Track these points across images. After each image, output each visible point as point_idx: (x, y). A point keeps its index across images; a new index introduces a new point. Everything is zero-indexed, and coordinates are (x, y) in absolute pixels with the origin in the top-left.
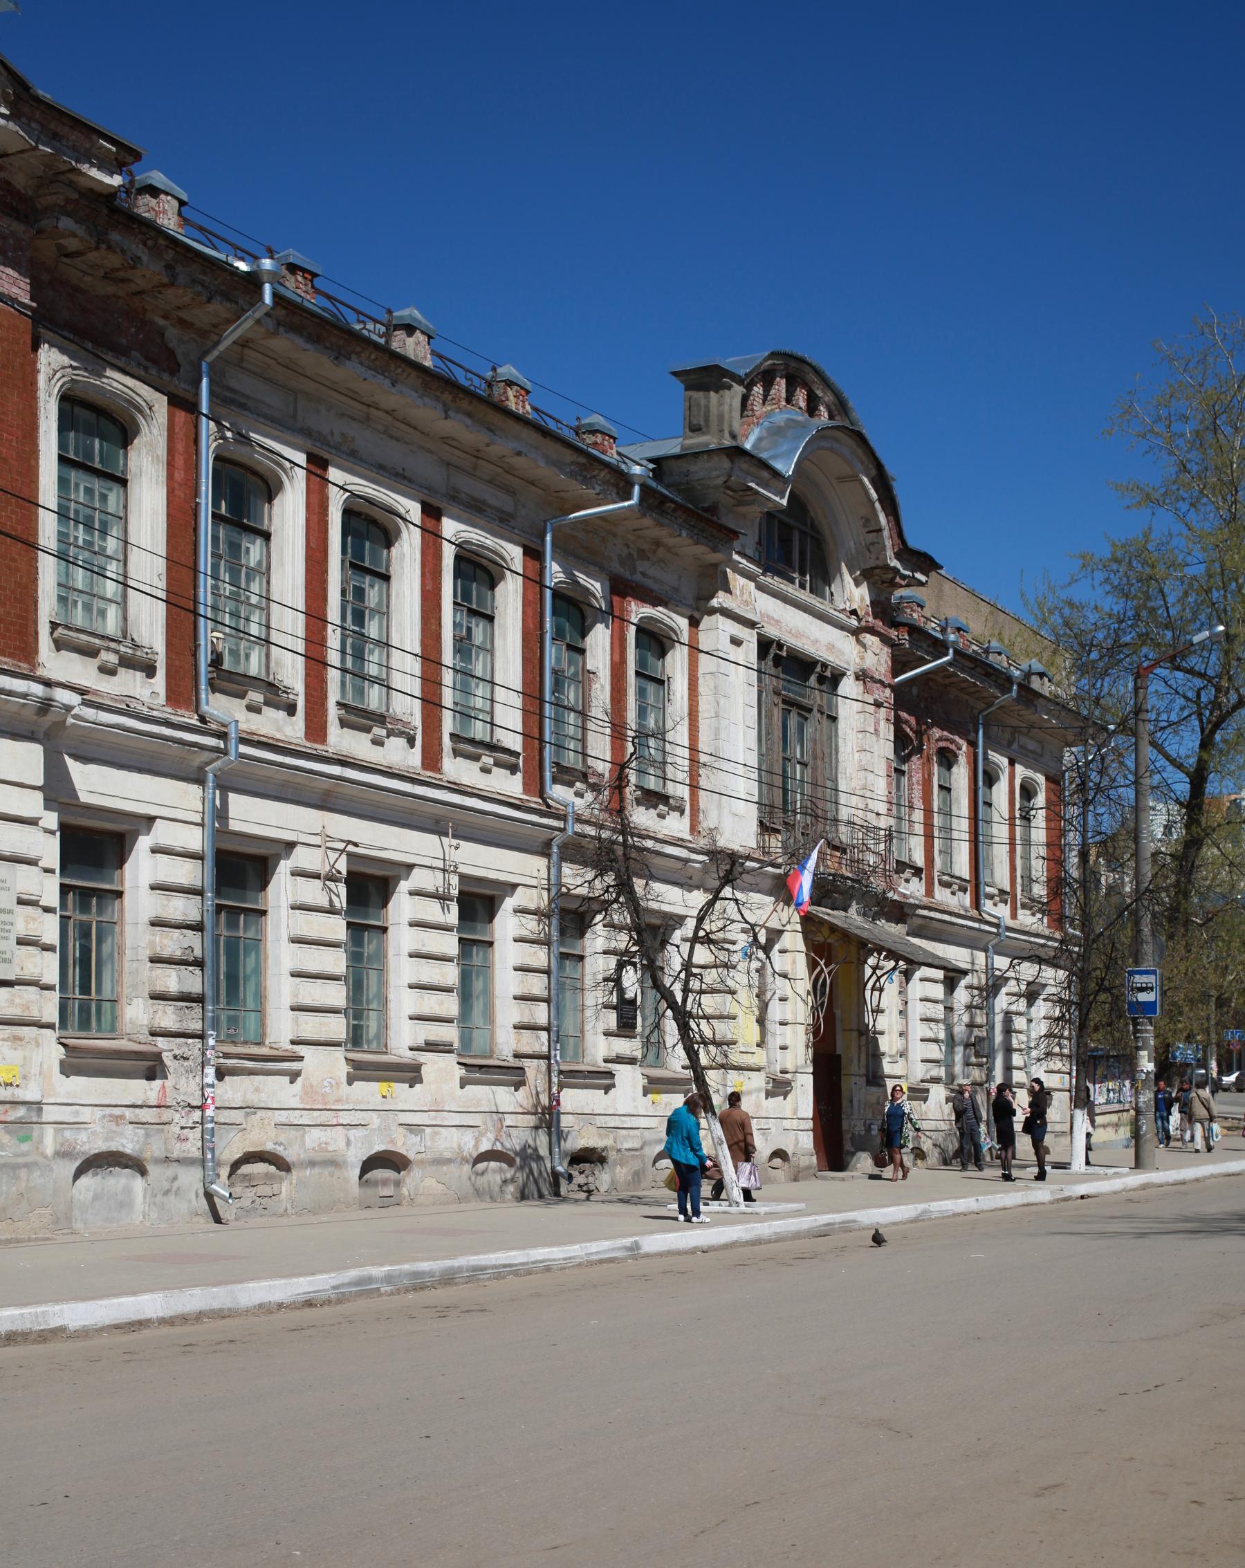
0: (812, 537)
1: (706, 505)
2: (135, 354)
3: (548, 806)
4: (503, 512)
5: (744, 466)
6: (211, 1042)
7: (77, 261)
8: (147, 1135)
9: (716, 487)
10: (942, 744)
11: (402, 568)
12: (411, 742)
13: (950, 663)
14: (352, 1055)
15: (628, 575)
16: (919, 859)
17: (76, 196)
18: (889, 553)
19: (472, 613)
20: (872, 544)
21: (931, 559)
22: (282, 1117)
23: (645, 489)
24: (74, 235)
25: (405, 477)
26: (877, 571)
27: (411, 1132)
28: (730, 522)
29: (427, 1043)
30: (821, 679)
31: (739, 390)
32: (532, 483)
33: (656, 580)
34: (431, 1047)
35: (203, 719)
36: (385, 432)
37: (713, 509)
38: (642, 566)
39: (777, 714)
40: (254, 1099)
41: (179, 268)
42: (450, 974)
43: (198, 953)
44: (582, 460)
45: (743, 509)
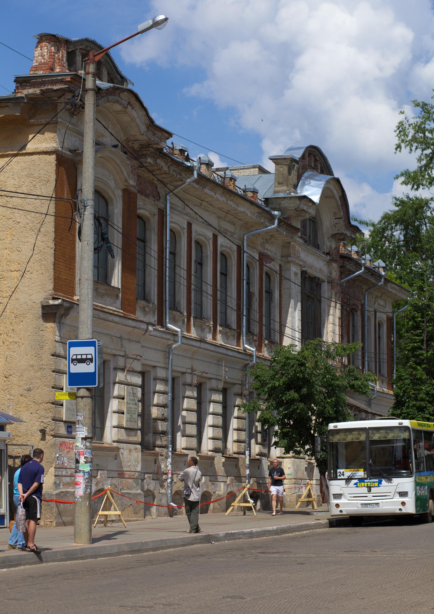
0: (313, 221)
1: (285, 216)
2: (151, 197)
4: (232, 233)
9: (291, 210)
10: (353, 307)
11: (207, 261)
13: (363, 273)
15: (263, 251)
20: (337, 224)
23: (280, 221)
26: (337, 235)
32: (240, 220)
36: (204, 209)
38: (267, 246)
41: (171, 167)
44: (260, 211)
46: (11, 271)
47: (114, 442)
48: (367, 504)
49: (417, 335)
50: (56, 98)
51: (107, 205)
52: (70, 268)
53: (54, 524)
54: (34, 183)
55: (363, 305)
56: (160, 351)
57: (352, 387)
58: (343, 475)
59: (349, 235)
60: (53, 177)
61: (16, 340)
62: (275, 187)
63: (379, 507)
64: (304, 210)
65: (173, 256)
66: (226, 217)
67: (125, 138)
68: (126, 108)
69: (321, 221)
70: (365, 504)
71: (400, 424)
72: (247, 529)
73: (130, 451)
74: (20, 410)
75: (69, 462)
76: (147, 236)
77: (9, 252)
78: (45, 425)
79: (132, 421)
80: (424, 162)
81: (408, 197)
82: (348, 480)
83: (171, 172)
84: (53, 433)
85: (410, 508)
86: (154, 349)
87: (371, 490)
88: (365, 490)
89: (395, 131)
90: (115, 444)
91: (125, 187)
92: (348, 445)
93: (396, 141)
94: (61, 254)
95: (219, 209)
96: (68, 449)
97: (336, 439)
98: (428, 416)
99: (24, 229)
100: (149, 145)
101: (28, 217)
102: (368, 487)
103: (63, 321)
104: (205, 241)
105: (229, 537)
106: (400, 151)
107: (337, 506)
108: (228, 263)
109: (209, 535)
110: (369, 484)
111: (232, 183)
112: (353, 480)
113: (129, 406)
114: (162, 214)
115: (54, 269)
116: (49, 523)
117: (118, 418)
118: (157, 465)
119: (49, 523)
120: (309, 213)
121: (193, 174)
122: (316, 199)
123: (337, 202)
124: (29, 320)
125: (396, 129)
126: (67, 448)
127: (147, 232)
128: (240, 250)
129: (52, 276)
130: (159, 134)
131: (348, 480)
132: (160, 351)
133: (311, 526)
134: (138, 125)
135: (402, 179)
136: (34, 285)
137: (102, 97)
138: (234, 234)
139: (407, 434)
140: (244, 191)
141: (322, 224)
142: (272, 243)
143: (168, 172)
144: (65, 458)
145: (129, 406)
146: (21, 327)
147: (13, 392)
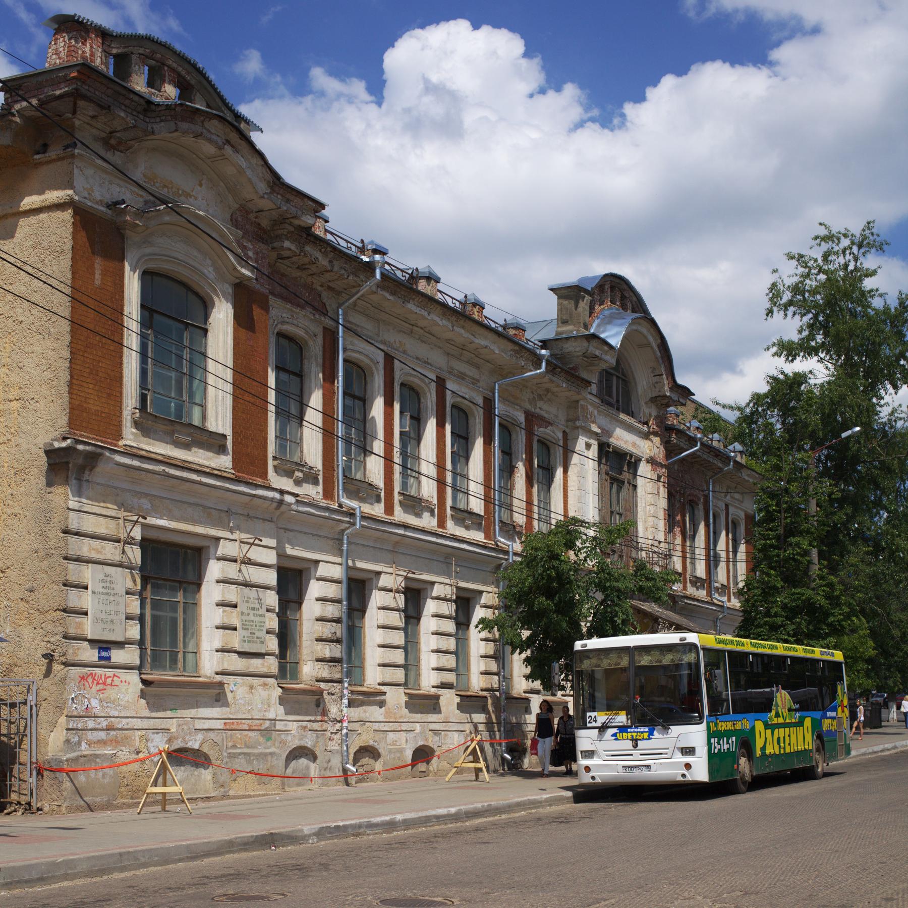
0: (623, 380)
3: (498, 546)
4: (473, 379)
5: (595, 344)
6: (346, 685)
7: (286, 262)
8: (317, 737)
9: (578, 357)
10: (690, 498)
12: (433, 515)
14: (407, 691)
15: (533, 410)
16: (680, 569)
17: (293, 229)
18: (667, 388)
19: (354, 397)
20: (657, 383)
21: (688, 390)
22: (376, 726)
23: (548, 363)
24: (290, 249)
25: (428, 364)
27: (435, 734)
28: (584, 375)
29: (442, 683)
30: (629, 463)
31: (588, 298)
32: (488, 361)
33: (547, 412)
34: (444, 686)
35: (340, 506)
36: (419, 339)
37: (575, 368)
38: (540, 404)
39: (607, 484)
40: (364, 716)
41: (335, 262)
42: (339, 630)
43: (339, 635)
44: (516, 348)
45: (591, 368)
46: (10, 401)
47: (217, 674)
48: (632, 767)
49: (771, 530)
50: (70, 116)
51: (510, 435)
52: (109, 395)
53: (63, 809)
54: (43, 257)
55: (707, 497)
56: (328, 538)
57: (641, 589)
58: (596, 721)
59: (676, 399)
60: (69, 243)
61: (17, 510)
62: (558, 326)
63: (650, 771)
64: (596, 357)
65: (415, 422)
66: (461, 355)
67: (237, 206)
68: (221, 148)
69: (634, 379)
70: (629, 767)
71: (681, 640)
72: (380, 816)
73: (251, 687)
74: (21, 623)
75: (102, 706)
76: (305, 367)
77: (7, 371)
78: (53, 647)
79: (254, 642)
80: (805, 333)
81: (783, 373)
82: (603, 728)
83: (336, 268)
84: (63, 659)
85: (700, 773)
86: (313, 535)
87: (637, 745)
88: (629, 744)
89: (767, 295)
90: (219, 678)
91: (238, 281)
92: (608, 673)
93: (768, 305)
94: (88, 370)
95: (448, 341)
96: (101, 687)
97: (586, 665)
98: (786, 637)
99: (28, 331)
100: (285, 219)
101: (34, 312)
102: (632, 740)
103: (86, 476)
104: (423, 385)
105: (330, 833)
106: (772, 317)
107: (588, 769)
108: (470, 422)
109: (272, 834)
110: (634, 734)
111: (475, 310)
112: (610, 730)
113: (245, 618)
114: (330, 338)
115: (70, 393)
116: (55, 808)
117: (223, 636)
118: (321, 708)
119: (55, 808)
120: (606, 361)
121: (374, 275)
122: (616, 341)
123: (654, 352)
124: (32, 478)
125: (768, 292)
126: (98, 683)
127: (305, 362)
128: (489, 404)
129: (66, 406)
130: (297, 200)
131: (603, 728)
132: (328, 538)
133: (541, 802)
134: (249, 180)
135: (774, 349)
136: (40, 420)
137: (162, 121)
138: (478, 381)
139: (693, 655)
140: (504, 329)
141: (636, 383)
142: (549, 400)
143: (329, 268)
144: (92, 700)
145: (245, 618)
146: (22, 489)
147: (11, 595)
